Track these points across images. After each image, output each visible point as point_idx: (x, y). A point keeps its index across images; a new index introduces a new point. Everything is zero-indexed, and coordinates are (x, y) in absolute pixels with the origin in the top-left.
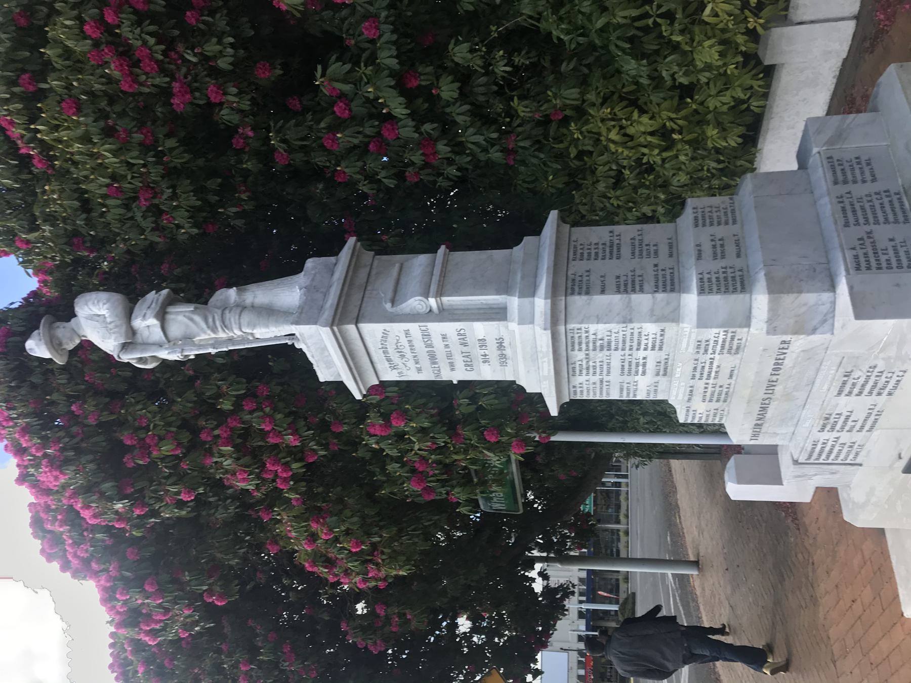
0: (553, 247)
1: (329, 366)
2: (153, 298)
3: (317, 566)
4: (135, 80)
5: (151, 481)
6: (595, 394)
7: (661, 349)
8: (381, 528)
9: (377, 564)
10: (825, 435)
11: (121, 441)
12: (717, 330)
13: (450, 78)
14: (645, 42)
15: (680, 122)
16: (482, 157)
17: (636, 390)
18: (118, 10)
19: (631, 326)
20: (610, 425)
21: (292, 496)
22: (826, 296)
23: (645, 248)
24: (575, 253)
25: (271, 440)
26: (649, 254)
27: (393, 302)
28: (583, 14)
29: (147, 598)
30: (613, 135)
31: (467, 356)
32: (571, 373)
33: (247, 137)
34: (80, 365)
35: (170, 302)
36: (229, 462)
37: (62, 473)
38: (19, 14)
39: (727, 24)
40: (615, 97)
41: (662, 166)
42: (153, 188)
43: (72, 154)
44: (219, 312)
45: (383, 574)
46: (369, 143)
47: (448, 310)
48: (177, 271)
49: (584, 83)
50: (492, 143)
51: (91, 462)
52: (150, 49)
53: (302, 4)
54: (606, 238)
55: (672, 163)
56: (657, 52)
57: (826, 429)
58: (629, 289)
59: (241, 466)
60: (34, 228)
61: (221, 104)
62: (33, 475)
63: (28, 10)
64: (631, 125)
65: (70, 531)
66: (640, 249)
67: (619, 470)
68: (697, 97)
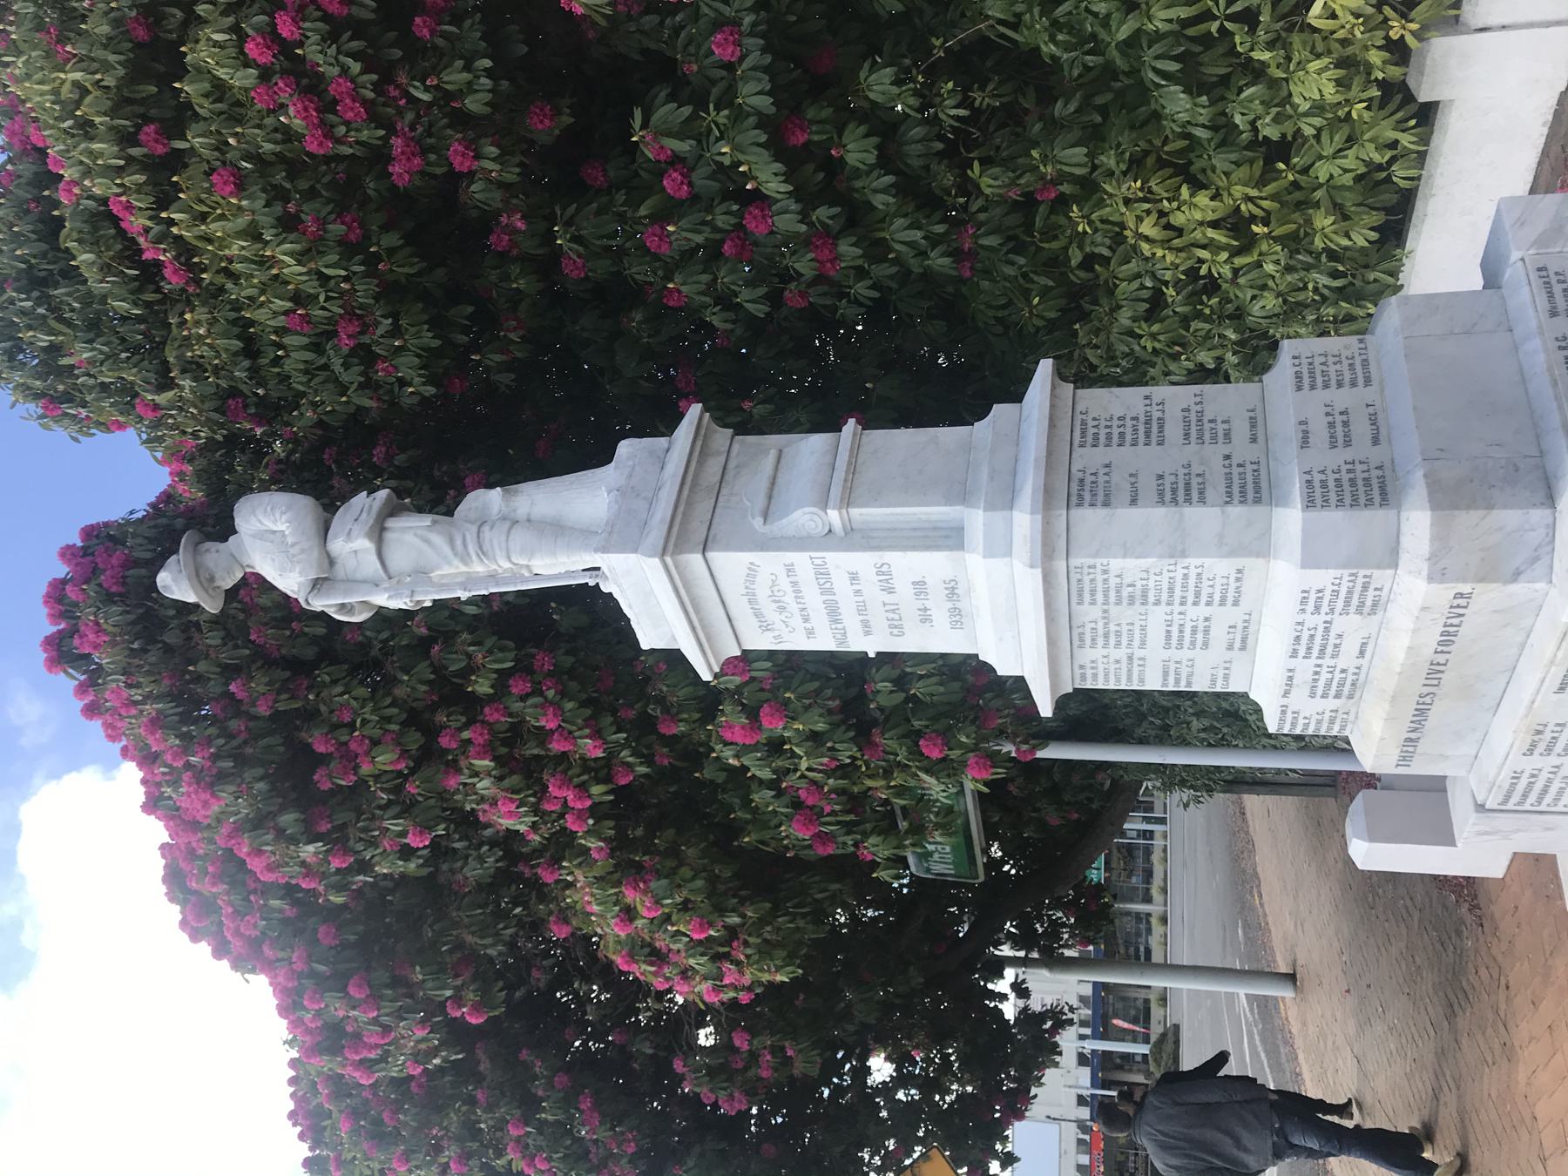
0: (1046, 423)
1: (657, 623)
2: (364, 504)
3: (636, 962)
4: (329, 134)
5: (359, 813)
6: (1118, 680)
7: (1236, 603)
8: (742, 902)
9: (738, 963)
10: (1536, 761)
11: (309, 745)
12: (1338, 573)
13: (862, 129)
14: (1211, 64)
15: (1266, 204)
16: (915, 265)
17: (1191, 675)
18: (300, 14)
19: (1186, 562)
20: (1139, 732)
21: (593, 844)
22: (1538, 515)
23: (1207, 426)
24: (1084, 433)
25: (556, 747)
26: (1214, 438)
27: (766, 516)
28: (1096, 15)
29: (354, 1008)
30: (1147, 228)
31: (893, 611)
32: (1076, 642)
33: (516, 231)
34: (241, 616)
35: (391, 511)
36: (486, 783)
37: (213, 795)
38: (136, 19)
39: (1351, 32)
40: (1150, 161)
41: (1234, 281)
42: (360, 317)
43: (230, 260)
44: (474, 529)
45: (747, 979)
46: (723, 241)
47: (861, 530)
48: (400, 459)
49: (1094, 138)
50: (934, 241)
51: (261, 779)
52: (352, 81)
53: (609, 4)
54: (1139, 409)
55: (1249, 276)
56: (1225, 80)
57: (1536, 752)
58: (1181, 498)
59: (506, 790)
60: (165, 384)
61: (471, 175)
62: (170, 798)
63: (151, 14)
64: (1179, 208)
65: (228, 893)
66: (1197, 428)
67: (1151, 810)
68: (1296, 160)
